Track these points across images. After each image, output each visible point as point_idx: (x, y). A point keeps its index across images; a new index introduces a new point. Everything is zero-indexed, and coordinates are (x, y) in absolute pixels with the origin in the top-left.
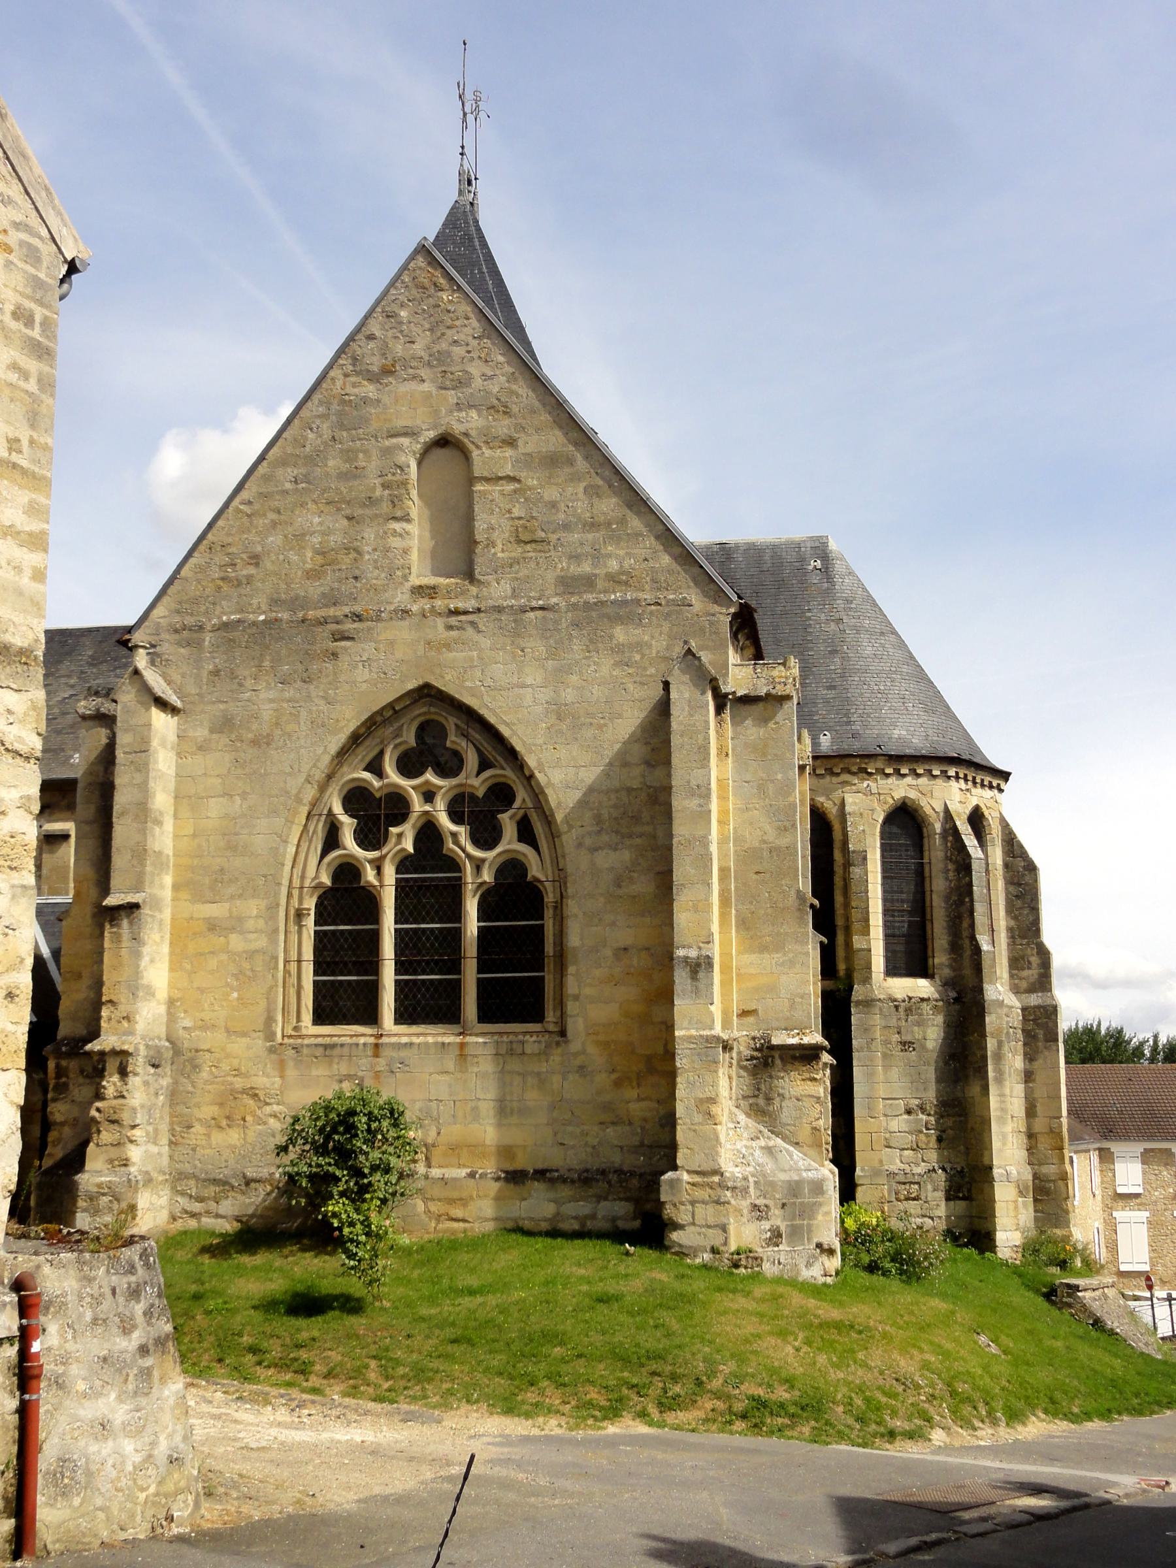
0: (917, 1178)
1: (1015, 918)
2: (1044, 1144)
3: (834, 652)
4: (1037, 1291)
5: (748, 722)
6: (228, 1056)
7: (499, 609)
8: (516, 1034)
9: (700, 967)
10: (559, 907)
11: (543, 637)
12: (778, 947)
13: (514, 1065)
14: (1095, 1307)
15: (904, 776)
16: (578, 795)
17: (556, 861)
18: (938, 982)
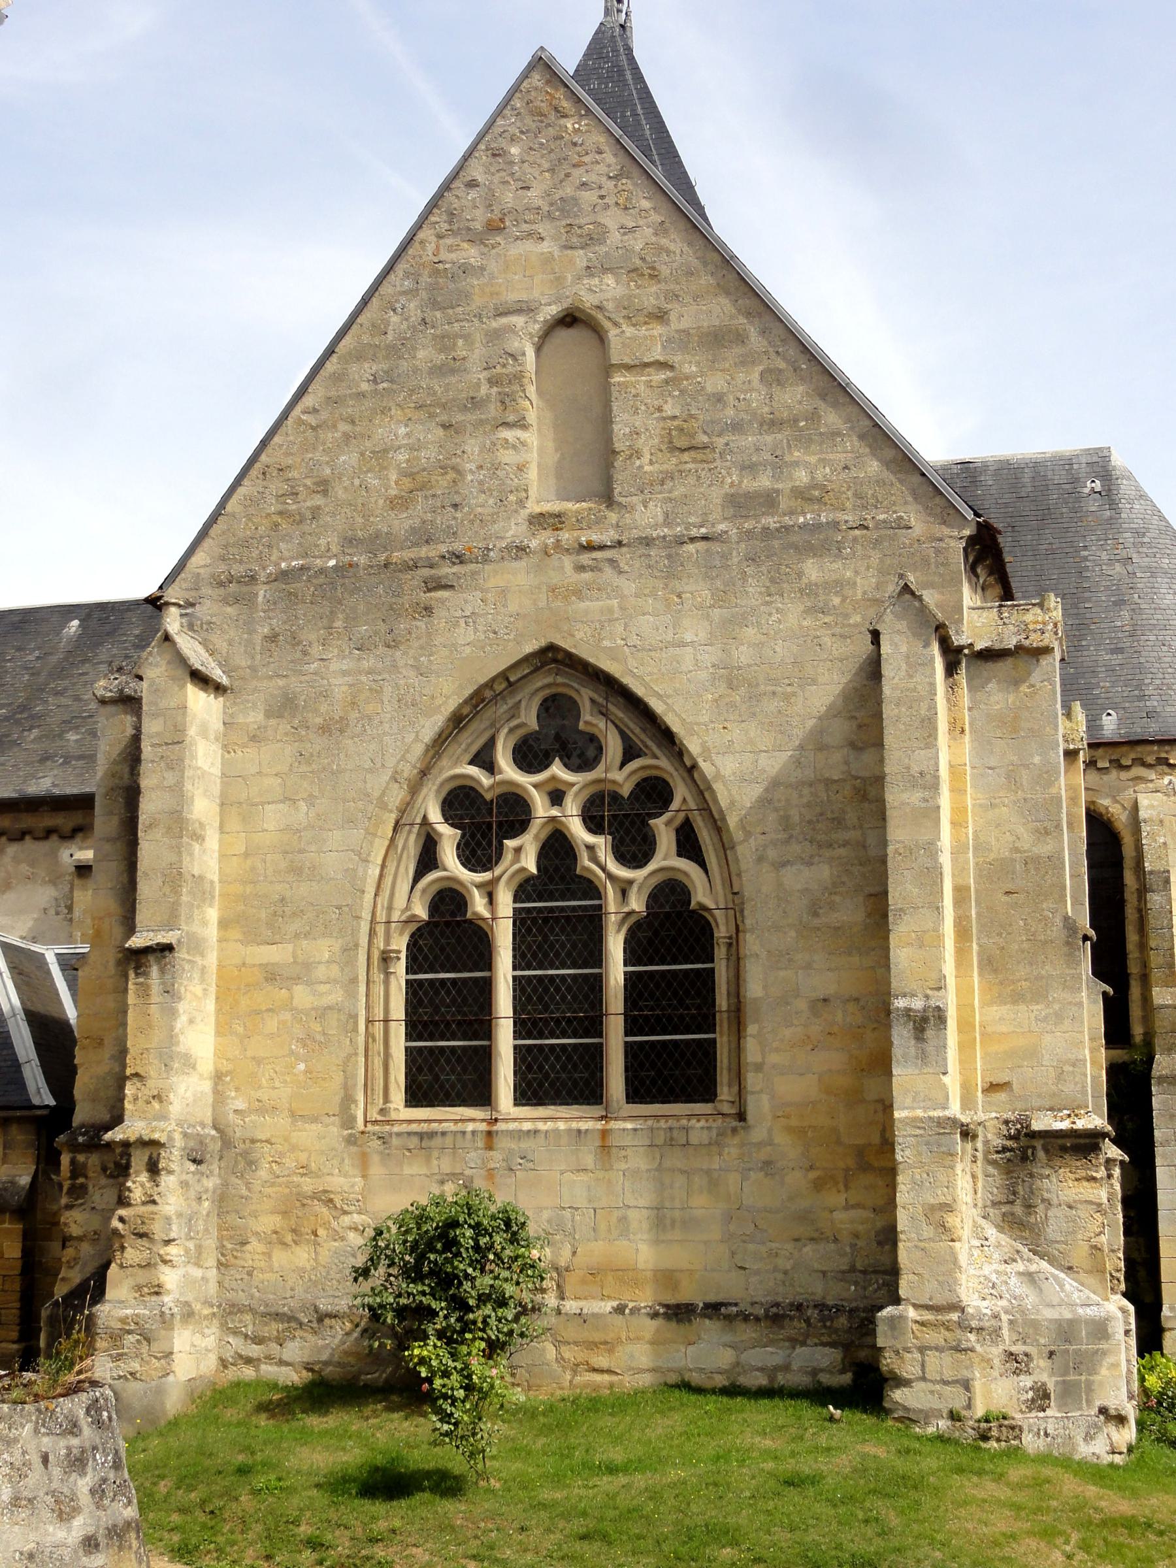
3: (1120, 603)
5: (992, 686)
6: (294, 1148)
7: (648, 542)
10: (734, 943)
11: (706, 576)
12: (1039, 995)
13: (676, 1160)
16: (757, 791)
17: (729, 882)
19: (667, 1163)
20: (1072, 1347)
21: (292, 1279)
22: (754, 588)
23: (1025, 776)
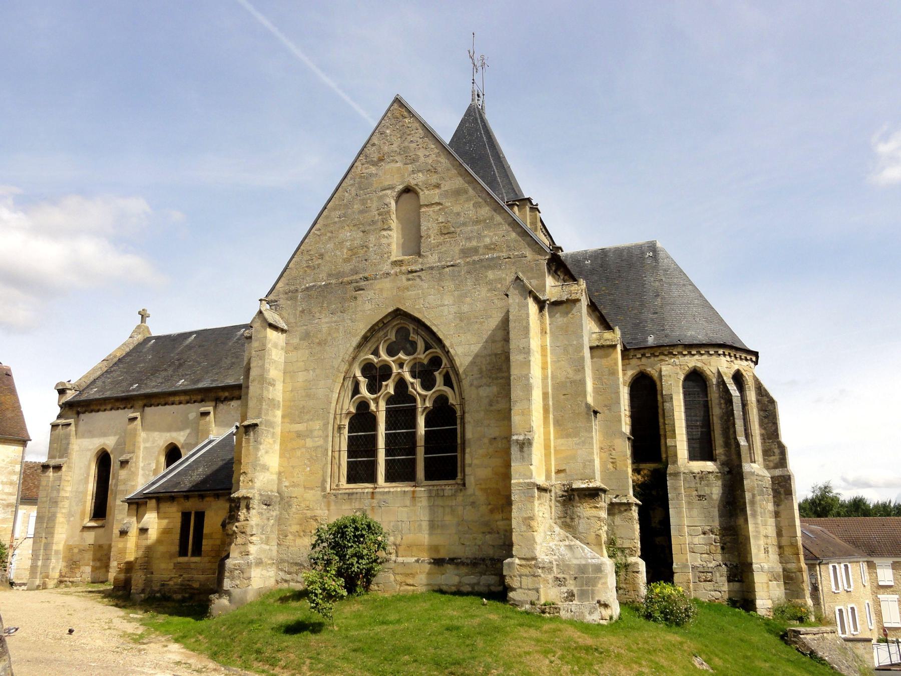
0: (710, 570)
1: (765, 429)
2: (788, 551)
3: (657, 296)
4: (777, 634)
5: (558, 315)
6: (304, 500)
7: (432, 268)
8: (441, 485)
9: (525, 445)
10: (463, 418)
11: (453, 280)
12: (576, 435)
13: (439, 502)
14: (814, 646)
15: (694, 355)
16: (470, 359)
17: (461, 394)
18: (718, 463)
19: (436, 503)
20: (586, 578)
21: (303, 550)
22: (469, 283)
23: (571, 350)
